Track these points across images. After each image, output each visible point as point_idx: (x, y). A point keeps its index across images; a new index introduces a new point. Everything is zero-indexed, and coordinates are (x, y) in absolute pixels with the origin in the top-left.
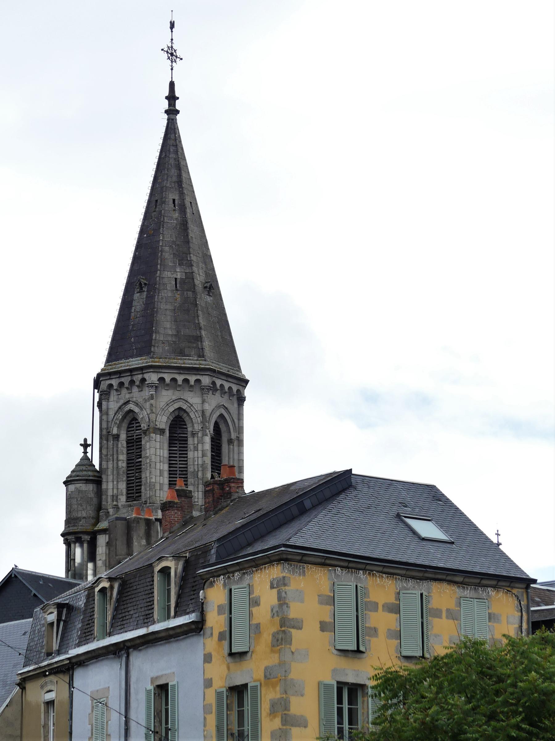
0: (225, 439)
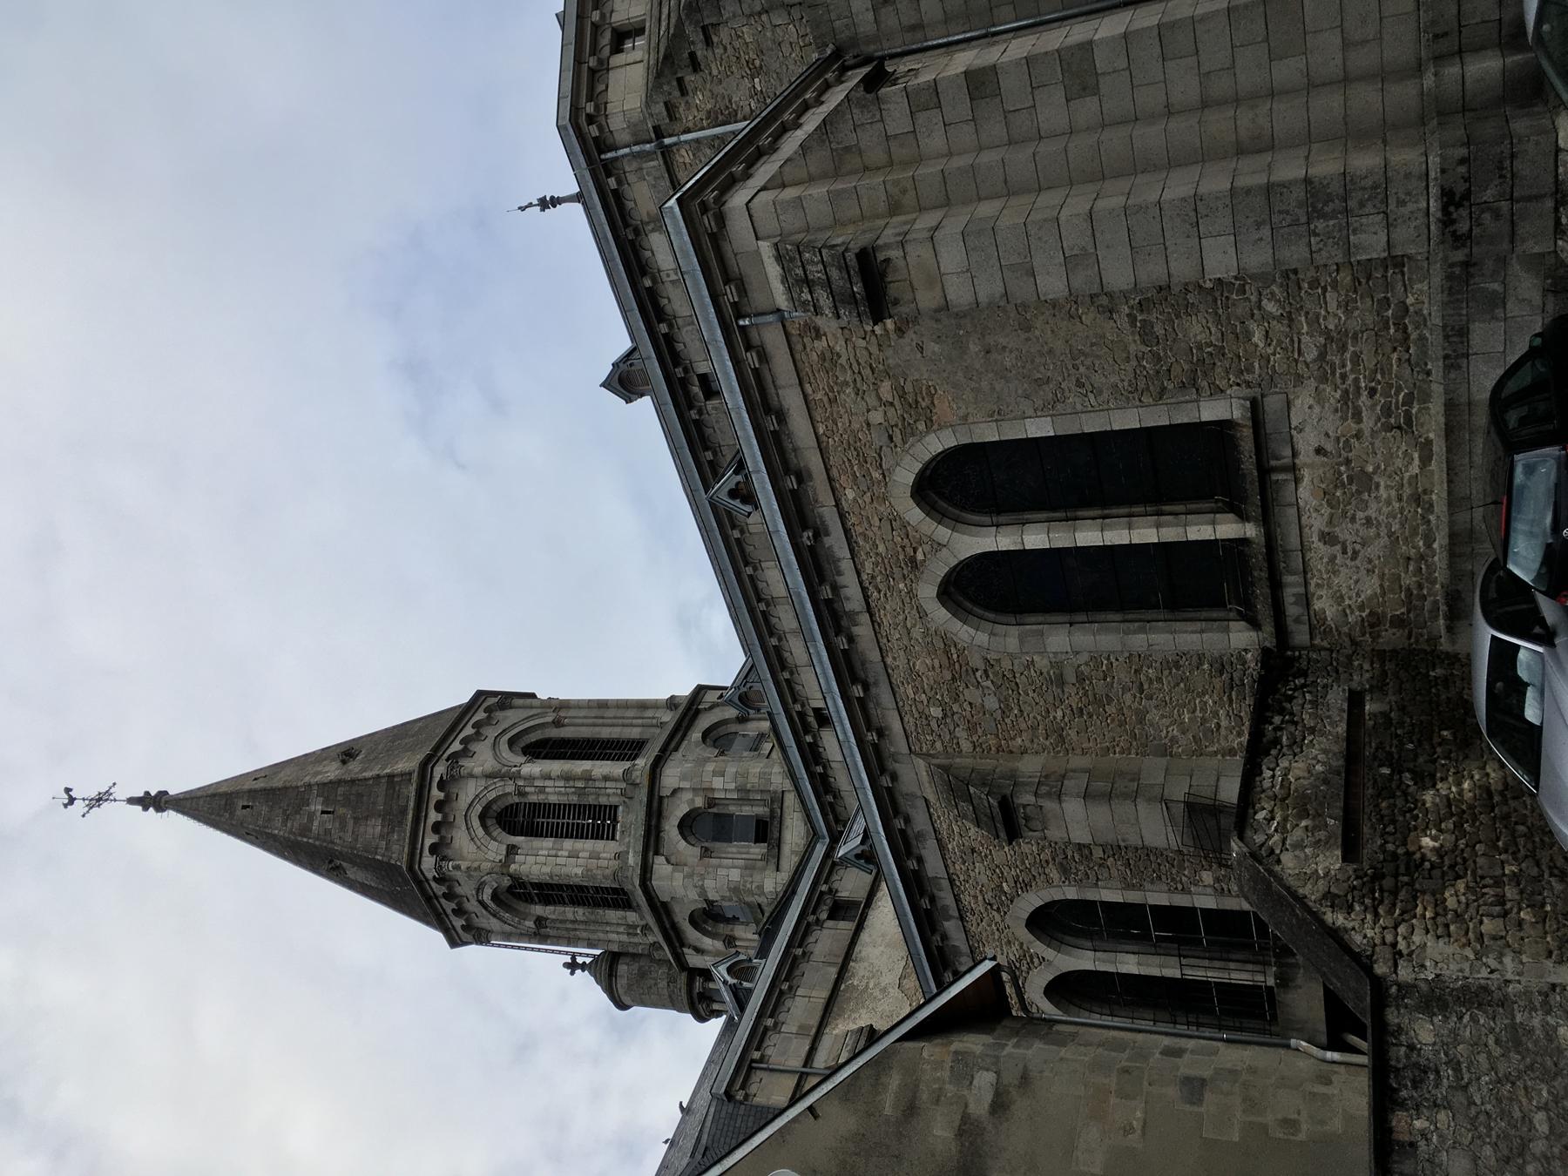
0: (555, 733)
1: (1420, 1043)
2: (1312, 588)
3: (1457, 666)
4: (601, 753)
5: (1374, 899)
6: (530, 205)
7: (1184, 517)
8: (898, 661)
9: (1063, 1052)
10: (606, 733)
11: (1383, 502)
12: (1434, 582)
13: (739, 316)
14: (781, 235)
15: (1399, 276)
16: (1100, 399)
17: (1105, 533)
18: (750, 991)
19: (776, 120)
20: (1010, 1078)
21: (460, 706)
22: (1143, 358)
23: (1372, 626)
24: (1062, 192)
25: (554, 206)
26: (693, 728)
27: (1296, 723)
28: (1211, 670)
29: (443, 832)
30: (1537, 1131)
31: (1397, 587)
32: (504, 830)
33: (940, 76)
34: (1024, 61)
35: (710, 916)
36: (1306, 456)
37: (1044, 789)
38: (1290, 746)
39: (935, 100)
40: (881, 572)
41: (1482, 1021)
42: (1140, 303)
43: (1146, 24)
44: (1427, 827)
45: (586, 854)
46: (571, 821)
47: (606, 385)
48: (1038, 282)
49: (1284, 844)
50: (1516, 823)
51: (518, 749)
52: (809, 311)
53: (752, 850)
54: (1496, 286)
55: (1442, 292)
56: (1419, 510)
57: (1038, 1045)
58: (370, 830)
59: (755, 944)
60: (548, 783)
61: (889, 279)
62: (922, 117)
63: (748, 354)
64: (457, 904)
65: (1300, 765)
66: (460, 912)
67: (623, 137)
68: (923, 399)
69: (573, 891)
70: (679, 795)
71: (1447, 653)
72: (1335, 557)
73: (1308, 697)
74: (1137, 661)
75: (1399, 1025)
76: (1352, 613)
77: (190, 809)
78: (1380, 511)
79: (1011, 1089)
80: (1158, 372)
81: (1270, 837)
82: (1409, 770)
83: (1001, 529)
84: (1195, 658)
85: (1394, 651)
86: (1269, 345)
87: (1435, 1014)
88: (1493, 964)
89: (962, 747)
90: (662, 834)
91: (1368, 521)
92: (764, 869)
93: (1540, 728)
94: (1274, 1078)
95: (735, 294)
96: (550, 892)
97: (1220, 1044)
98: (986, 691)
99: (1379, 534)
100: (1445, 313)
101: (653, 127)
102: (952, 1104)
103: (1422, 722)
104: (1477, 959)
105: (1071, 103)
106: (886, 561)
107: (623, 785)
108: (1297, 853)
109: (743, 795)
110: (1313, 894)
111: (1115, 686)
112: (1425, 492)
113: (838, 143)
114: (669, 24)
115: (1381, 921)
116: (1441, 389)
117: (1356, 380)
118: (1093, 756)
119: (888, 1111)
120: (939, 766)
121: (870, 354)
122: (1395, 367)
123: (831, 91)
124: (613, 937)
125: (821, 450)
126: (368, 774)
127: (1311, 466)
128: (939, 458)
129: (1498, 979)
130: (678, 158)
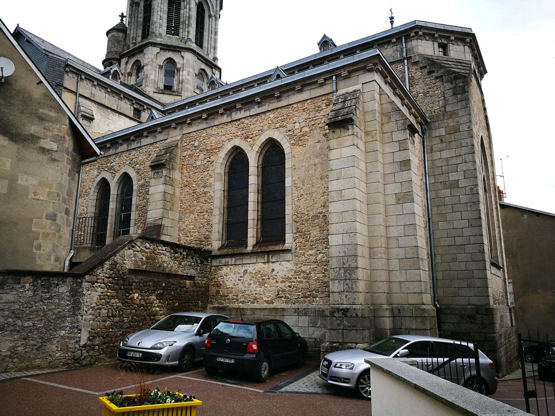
0: (207, 15)
2: (230, 267)
5: (115, 277)
8: (214, 131)
10: (206, 34)
11: (255, 288)
12: (229, 303)
13: (337, 76)
15: (325, 296)
16: (296, 202)
18: (108, 78)
20: (55, 155)
23: (217, 284)
24: (365, 191)
27: (183, 259)
35: (139, 67)
36: (271, 266)
37: (168, 179)
38: (174, 256)
41: (67, 307)
42: (326, 215)
43: (417, 220)
45: (161, 23)
47: (325, 36)
49: (136, 251)
50: (143, 323)
53: (161, 84)
54: (319, 325)
59: (129, 84)
60: (188, 10)
61: (342, 130)
62: (397, 144)
65: (167, 259)
70: (182, 58)
73: (193, 264)
74: (210, 211)
76: (222, 279)
78: (253, 288)
79: (50, 155)
81: (139, 247)
82: (164, 292)
83: (256, 168)
84: (210, 230)
85: (208, 291)
87: (70, 293)
88: (89, 312)
91: (250, 284)
93: (173, 331)
97: (72, 227)
98: (203, 161)
102: (44, 134)
105: (394, 195)
107: (186, 38)
109: (181, 81)
114: (445, 64)
117: (294, 282)
119: (41, 111)
120: (177, 143)
121: (319, 124)
123: (414, 119)
124: (132, 32)
125: (287, 105)
127: (269, 267)
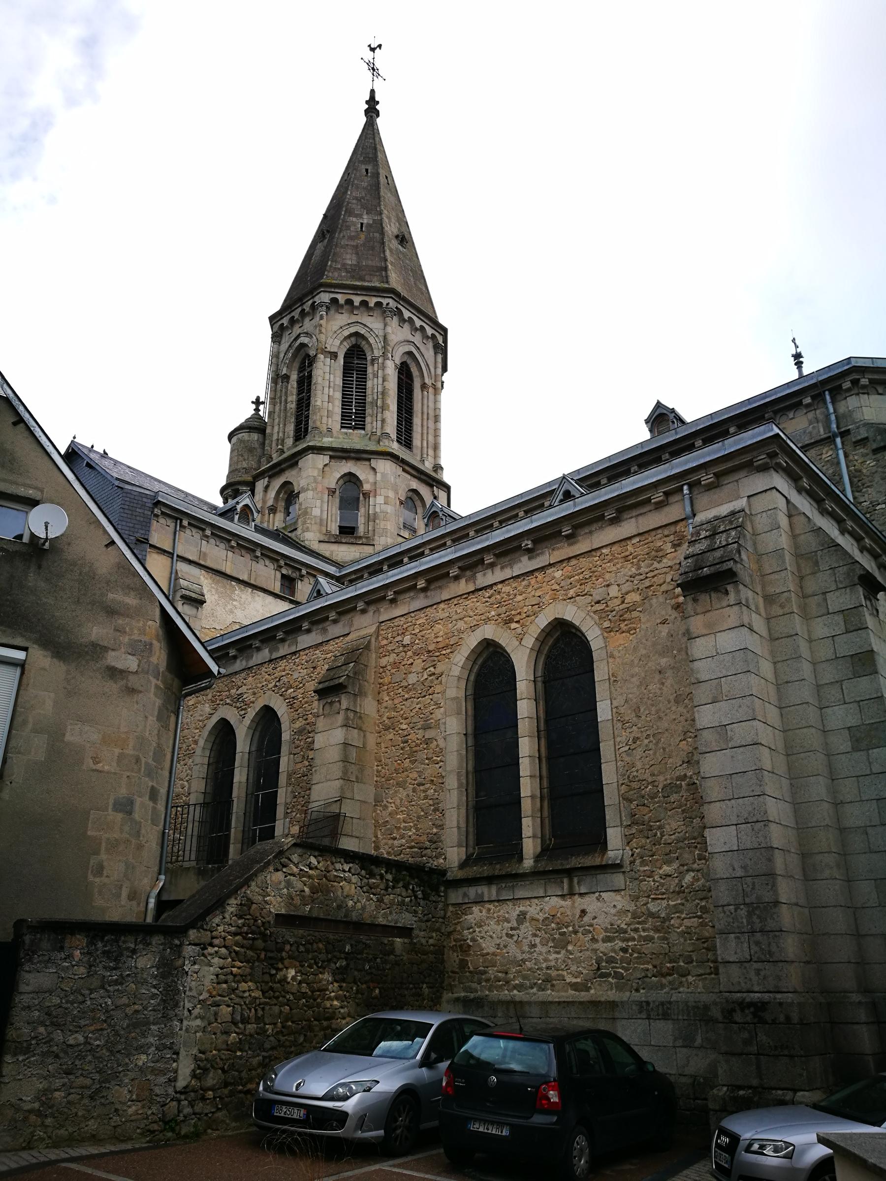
1: (137, 958)
2: (487, 906)
3: (430, 1003)
4: (402, 418)
5: (247, 933)
6: (797, 347)
7: (539, 815)
8: (442, 612)
9: (152, 719)
10: (417, 421)
12: (490, 990)
13: (691, 486)
14: (751, 514)
16: (624, 755)
17: (528, 759)
18: (232, 520)
19: (847, 516)
20: (133, 681)
21: (436, 317)
22: (653, 786)
23: (461, 946)
24: (777, 724)
25: (796, 364)
26: (419, 482)
27: (386, 889)
28: (432, 834)
29: (346, 307)
30: (70, 1036)
31: (487, 964)
32: (348, 350)
33: (870, 631)
34: (879, 695)
35: (289, 495)
37: (351, 715)
38: (368, 884)
39: (852, 629)
40: (503, 598)
41: (152, 1002)
42: (694, 783)
44: (303, 974)
46: (354, 397)
47: (659, 405)
48: (708, 706)
49: (291, 875)
50: (305, 1036)
51: (406, 358)
52: (692, 537)
53: (333, 524)
54: (699, 1041)
55: (695, 1002)
56: (540, 982)
57: (158, 702)
58: (348, 256)
59: (271, 528)
60: (380, 380)
62: (839, 618)
63: (661, 494)
64: (297, 319)
65: (353, 890)
66: (293, 321)
67: (842, 407)
68: (626, 625)
69: (307, 400)
70: (372, 472)
71: (441, 997)
72: (509, 922)
73: (408, 900)
74: (439, 782)
75: (150, 944)
76: (470, 933)
77: (367, 134)
80: (643, 797)
81: (296, 865)
82: (348, 965)
84: (440, 823)
85: (443, 962)
86: (661, 877)
87: (158, 969)
88: (196, 1012)
89: (383, 659)
90: (344, 461)
92: (320, 532)
93: (370, 1055)
94: (133, 861)
95: (707, 481)
96: (305, 384)
97: (161, 827)
99: (524, 953)
100: (680, 1003)
101: (849, 429)
102: (115, 640)
103: (386, 976)
104: (200, 1001)
106: (510, 601)
107: (379, 434)
108: (283, 884)
109: (371, 517)
110: (251, 892)
111: (423, 766)
112: (553, 986)
113: (821, 556)
115: (230, 937)
116: (625, 999)
117: (633, 939)
118: (376, 751)
119: (111, 596)
120: (369, 642)
121: (660, 585)
122: (642, 966)
123: (872, 560)
124: (276, 429)
125: (590, 551)
126: (388, 253)
127: (573, 906)
128: (583, 638)
129: (183, 1014)
130: (826, 449)
